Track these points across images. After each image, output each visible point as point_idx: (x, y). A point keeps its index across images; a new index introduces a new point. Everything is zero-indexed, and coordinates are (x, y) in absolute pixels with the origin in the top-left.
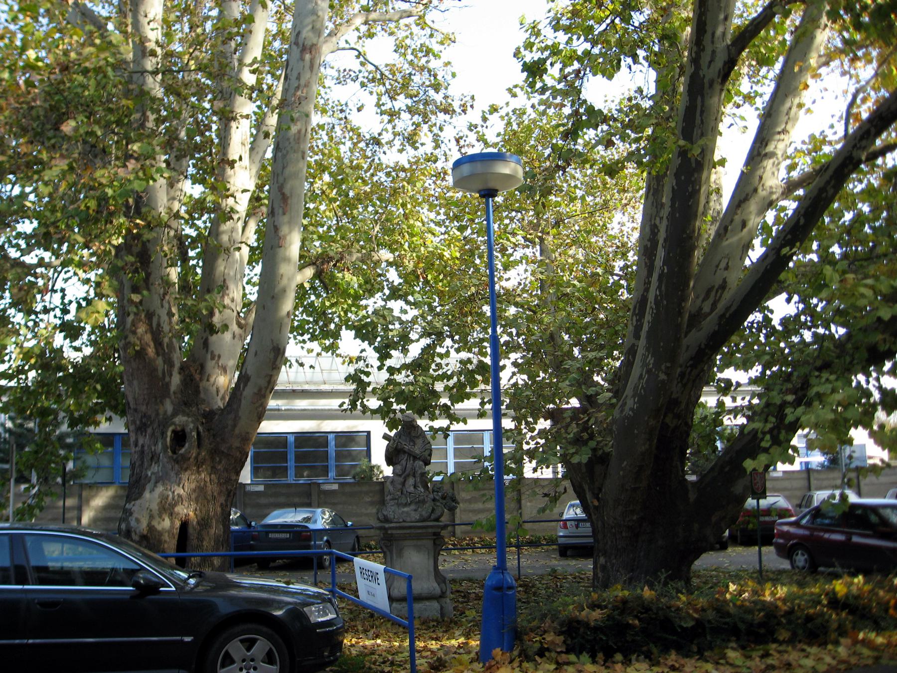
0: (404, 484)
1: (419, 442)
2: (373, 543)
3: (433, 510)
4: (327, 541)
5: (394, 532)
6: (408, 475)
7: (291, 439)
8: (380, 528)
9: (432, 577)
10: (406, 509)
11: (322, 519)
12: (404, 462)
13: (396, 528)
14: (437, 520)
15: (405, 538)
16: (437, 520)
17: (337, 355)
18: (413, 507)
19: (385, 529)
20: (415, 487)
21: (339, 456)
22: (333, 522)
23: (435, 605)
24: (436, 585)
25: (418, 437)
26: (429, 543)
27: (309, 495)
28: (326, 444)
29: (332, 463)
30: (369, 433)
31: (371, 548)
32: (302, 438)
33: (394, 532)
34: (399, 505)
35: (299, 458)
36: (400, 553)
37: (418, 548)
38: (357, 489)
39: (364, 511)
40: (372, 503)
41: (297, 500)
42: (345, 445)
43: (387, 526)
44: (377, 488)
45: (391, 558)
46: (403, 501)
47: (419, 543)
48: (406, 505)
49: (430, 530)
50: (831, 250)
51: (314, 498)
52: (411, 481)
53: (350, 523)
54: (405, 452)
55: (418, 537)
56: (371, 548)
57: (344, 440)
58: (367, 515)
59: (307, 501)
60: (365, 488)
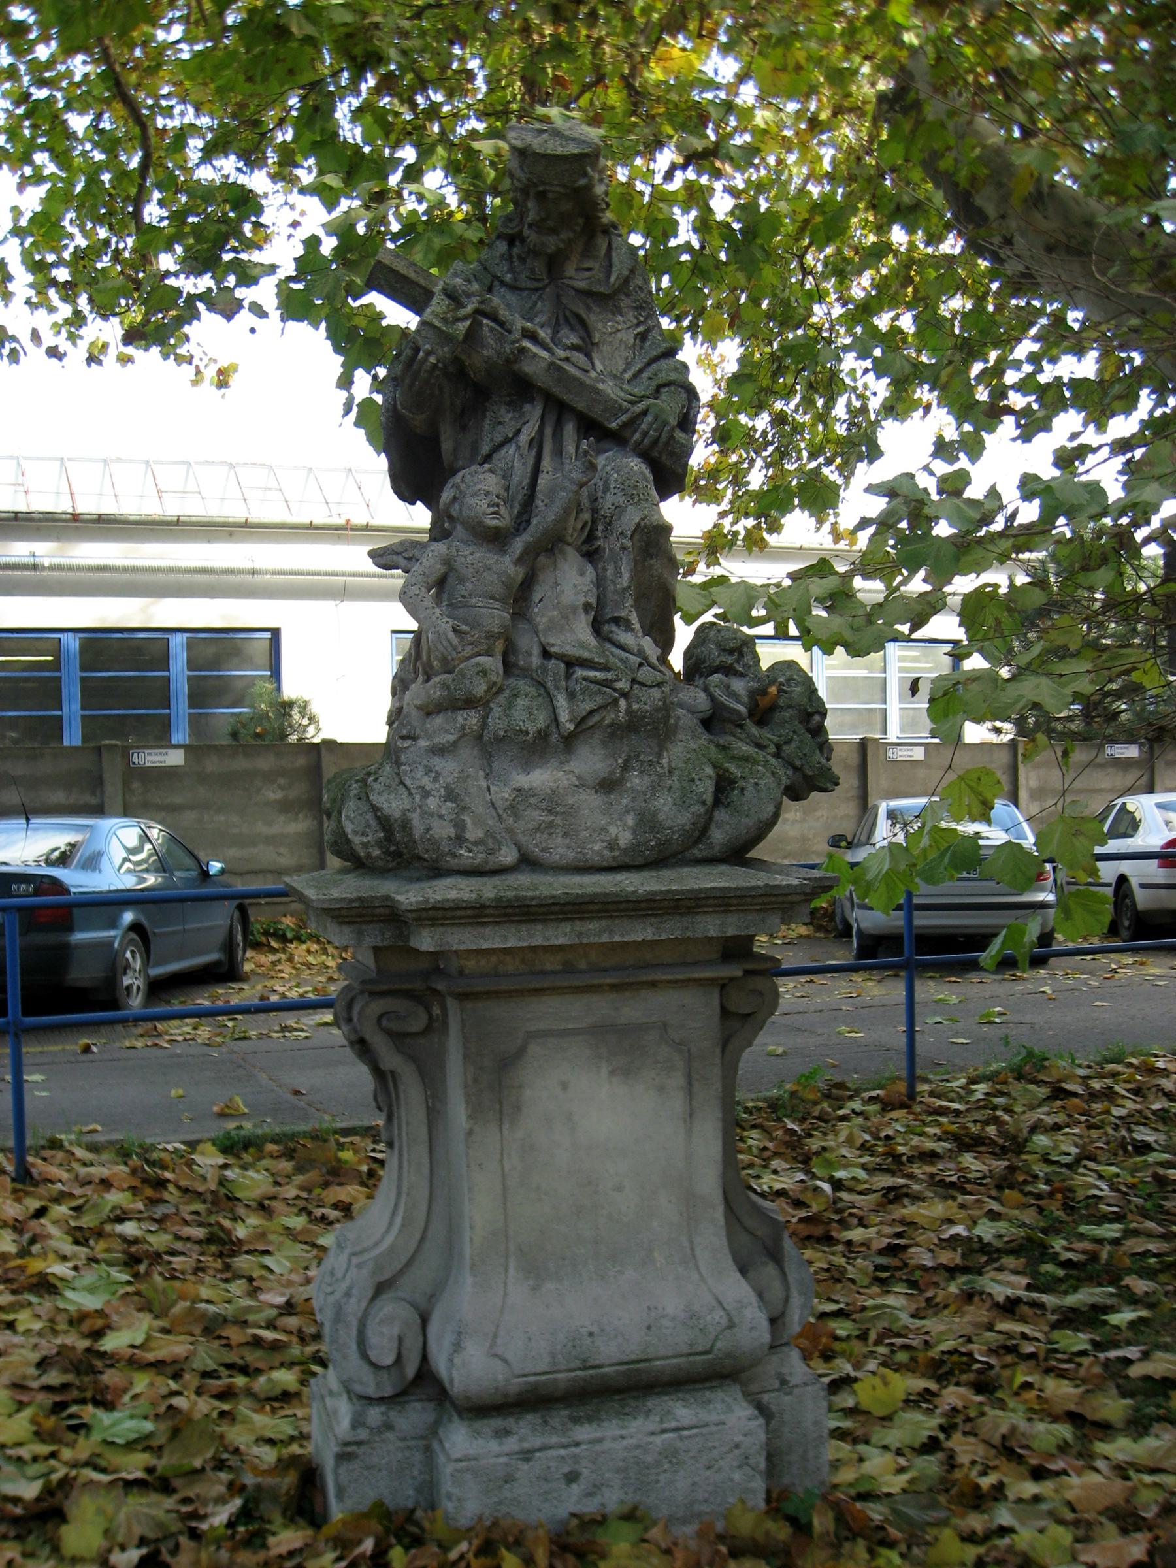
0: (520, 597)
1: (615, 332)
2: (289, 921)
3: (724, 785)
4: (135, 927)
5: (461, 939)
6: (550, 546)
7: (72, 644)
8: (355, 915)
9: (712, 1234)
10: (541, 778)
11: (120, 853)
12: (517, 459)
13: (477, 914)
14: (738, 854)
15: (535, 977)
16: (738, 854)
17: (180, 359)
18: (591, 761)
19: (392, 917)
20: (601, 622)
21: (200, 695)
22: (162, 865)
23: (732, 1417)
24: (736, 1289)
25: (606, 300)
26: (691, 1011)
27: (97, 782)
28: (163, 660)
29: (180, 707)
30: (276, 632)
31: (284, 939)
32: (100, 644)
33: (461, 939)
34: (489, 746)
35: (92, 693)
36: (498, 1082)
37: (621, 1047)
38: (241, 764)
39: (262, 828)
40: (286, 807)
41: (59, 797)
42: (215, 664)
43: (409, 895)
44: (301, 761)
45: (435, 1114)
46: (526, 714)
47: (632, 1010)
48: (541, 746)
49: (711, 926)
50: (1093, 355)
51: (113, 789)
52: (571, 582)
53: (215, 866)
54: (523, 389)
55: (628, 972)
56: (284, 939)
57: (211, 650)
58: (270, 840)
59: (93, 801)
60: (264, 763)
